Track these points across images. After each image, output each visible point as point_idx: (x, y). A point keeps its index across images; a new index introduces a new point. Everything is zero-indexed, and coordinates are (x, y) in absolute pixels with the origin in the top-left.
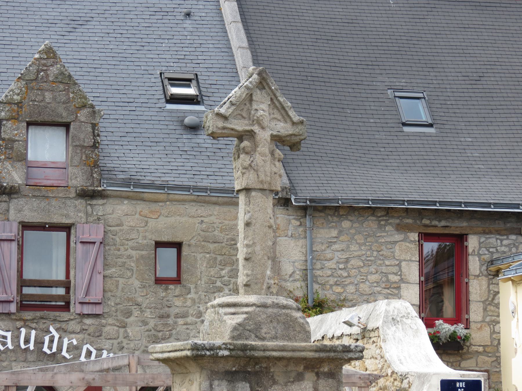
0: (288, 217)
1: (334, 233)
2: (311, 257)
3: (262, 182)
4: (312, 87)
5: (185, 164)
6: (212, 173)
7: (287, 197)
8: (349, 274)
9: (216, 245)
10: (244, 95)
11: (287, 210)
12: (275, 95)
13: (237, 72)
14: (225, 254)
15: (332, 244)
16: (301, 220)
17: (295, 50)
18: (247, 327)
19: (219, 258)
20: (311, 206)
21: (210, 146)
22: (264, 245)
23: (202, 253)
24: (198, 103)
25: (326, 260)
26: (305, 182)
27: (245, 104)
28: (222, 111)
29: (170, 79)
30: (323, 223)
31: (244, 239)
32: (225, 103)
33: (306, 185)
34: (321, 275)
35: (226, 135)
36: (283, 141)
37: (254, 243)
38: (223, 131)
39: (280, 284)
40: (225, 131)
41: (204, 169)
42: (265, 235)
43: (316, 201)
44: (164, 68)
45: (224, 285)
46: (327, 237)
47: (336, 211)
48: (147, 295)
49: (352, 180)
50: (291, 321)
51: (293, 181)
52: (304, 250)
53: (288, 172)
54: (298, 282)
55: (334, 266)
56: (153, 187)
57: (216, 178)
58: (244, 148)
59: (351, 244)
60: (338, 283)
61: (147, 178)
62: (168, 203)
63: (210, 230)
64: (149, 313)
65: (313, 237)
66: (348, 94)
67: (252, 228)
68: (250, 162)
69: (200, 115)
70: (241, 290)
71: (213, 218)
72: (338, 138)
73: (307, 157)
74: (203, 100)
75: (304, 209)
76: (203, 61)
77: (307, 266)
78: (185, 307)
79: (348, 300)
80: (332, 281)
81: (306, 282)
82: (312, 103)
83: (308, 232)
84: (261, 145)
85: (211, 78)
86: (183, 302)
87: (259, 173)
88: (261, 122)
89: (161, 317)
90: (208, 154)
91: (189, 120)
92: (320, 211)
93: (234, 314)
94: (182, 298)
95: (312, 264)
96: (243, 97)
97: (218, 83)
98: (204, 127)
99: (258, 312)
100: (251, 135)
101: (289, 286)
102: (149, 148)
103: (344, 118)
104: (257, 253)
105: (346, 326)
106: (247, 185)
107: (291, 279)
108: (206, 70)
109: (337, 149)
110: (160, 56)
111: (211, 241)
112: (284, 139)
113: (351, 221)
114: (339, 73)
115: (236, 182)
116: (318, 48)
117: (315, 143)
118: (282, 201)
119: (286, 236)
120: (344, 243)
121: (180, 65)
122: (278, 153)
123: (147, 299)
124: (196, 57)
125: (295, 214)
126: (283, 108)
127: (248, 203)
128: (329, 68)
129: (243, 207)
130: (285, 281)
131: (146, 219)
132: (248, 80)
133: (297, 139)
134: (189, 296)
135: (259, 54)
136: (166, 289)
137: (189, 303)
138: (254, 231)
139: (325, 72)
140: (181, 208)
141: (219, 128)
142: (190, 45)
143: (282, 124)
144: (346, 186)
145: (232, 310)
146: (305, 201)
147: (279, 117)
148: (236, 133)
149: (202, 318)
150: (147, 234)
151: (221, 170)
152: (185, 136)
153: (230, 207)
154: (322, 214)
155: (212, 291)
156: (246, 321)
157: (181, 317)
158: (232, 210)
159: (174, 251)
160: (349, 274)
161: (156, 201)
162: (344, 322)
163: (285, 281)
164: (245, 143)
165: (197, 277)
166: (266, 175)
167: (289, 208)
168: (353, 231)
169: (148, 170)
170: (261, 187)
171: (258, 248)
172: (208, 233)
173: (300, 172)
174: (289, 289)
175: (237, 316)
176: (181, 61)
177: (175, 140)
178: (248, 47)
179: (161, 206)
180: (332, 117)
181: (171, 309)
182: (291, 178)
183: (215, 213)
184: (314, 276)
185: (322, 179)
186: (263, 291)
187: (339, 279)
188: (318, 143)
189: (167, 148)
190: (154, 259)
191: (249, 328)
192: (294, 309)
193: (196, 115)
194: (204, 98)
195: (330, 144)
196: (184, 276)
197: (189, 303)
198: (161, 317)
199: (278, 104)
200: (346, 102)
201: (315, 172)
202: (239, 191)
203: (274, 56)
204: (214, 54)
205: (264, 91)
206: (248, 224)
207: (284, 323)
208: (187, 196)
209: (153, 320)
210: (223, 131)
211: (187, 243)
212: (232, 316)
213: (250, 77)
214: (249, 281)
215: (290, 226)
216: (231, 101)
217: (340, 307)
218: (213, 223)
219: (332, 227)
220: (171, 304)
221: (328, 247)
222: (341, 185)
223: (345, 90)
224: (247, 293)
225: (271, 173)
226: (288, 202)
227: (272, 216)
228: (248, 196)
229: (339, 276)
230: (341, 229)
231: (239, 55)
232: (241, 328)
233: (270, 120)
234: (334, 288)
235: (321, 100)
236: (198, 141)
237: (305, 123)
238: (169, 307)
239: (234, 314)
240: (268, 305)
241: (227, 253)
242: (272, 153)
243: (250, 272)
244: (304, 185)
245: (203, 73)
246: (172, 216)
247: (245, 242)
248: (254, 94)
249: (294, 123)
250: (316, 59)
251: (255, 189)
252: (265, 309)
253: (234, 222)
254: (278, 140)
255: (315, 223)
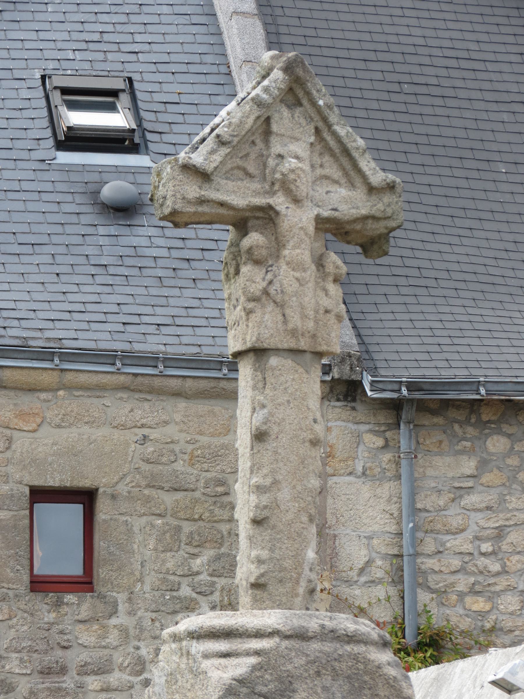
0: (354, 427)
1: (469, 465)
2: (411, 525)
3: (294, 333)
4: (413, 109)
5: (104, 298)
6: (169, 321)
7: (354, 377)
8: (504, 566)
9: (179, 495)
10: (250, 121)
11: (353, 409)
12: (325, 120)
13: (229, 74)
14: (200, 519)
15: (462, 492)
16: (388, 434)
17: (370, 18)
18: (260, 688)
19: (187, 527)
20: (411, 401)
21: (164, 253)
22: (299, 488)
23: (144, 514)
24: (134, 149)
25: (448, 532)
26: (396, 340)
27: (253, 142)
28: (198, 158)
29: (65, 91)
30: (441, 442)
31: (252, 472)
32: (203, 140)
33: (400, 348)
34: (437, 569)
35: (207, 218)
36: (346, 233)
37: (275, 482)
38: (200, 209)
39: (335, 591)
40: (205, 209)
41: (148, 310)
42: (303, 462)
43: (425, 387)
44: (51, 65)
45: (199, 593)
46: (450, 475)
47: (472, 411)
48: (10, 619)
49: (511, 335)
50: (366, 672)
51: (367, 340)
52: (394, 508)
53: (354, 317)
54: (379, 587)
55: (468, 547)
56: (26, 355)
57: (179, 331)
58: (250, 251)
59: (509, 494)
60: (477, 588)
61: (11, 332)
62: (61, 393)
63: (164, 459)
64: (17, 662)
65: (416, 475)
66: (499, 127)
67: (271, 444)
68: (264, 284)
69: (141, 179)
70: (245, 598)
71: (171, 430)
72: (476, 233)
73: (402, 281)
74: (146, 141)
75: (395, 406)
76: (147, 47)
77: (401, 546)
78: (105, 647)
79: (501, 629)
80: (463, 583)
81: (400, 587)
82: (413, 148)
83: (404, 463)
84: (291, 243)
85: (166, 87)
86: (99, 637)
87: (288, 311)
88: (292, 187)
89: (46, 672)
90: (160, 273)
91: (110, 191)
92: (434, 413)
93: (226, 655)
94: (96, 627)
95: (415, 542)
96: (248, 126)
97: (184, 99)
98: (151, 200)
99: (286, 652)
100: (267, 216)
101: (359, 595)
102: (16, 259)
103: (490, 186)
104: (282, 507)
105: (498, 691)
106: (258, 339)
107: (363, 579)
108: (153, 68)
109: (474, 260)
110: (42, 35)
111: (167, 486)
112: (348, 227)
113: (509, 436)
114: (480, 75)
115: (231, 334)
116: (426, 14)
117: (420, 245)
118: (342, 388)
119: (350, 474)
120: (492, 491)
121: (89, 56)
122: (333, 259)
123: (10, 627)
124: (129, 38)
125: (372, 420)
126: (346, 152)
127: (261, 384)
128: (453, 63)
129: (249, 393)
130: (349, 582)
131: (8, 432)
132: (259, 83)
133: (380, 227)
134: (114, 621)
135: (283, 30)
136: (58, 604)
137: (113, 638)
138: (276, 453)
139: (443, 72)
140: (93, 405)
141: (189, 202)
142: (114, 9)
143: (343, 192)
144: (496, 350)
145: (222, 646)
146: (396, 387)
147: (336, 173)
148: (231, 213)
149: (145, 675)
150: (11, 469)
151: (192, 312)
152: (102, 230)
153: (213, 402)
154: (439, 420)
155: (170, 607)
156: (258, 674)
157: (96, 673)
158: (217, 409)
159: (76, 511)
160: (504, 566)
161: (32, 389)
162: (494, 683)
163: (349, 582)
164: (254, 238)
165: (132, 573)
166: (304, 317)
167: (358, 405)
168: (513, 461)
169: (12, 314)
170: (292, 345)
171: (284, 494)
172: (161, 467)
173: (383, 316)
174: (357, 604)
175: (233, 661)
176: (92, 46)
177: (79, 240)
178: (256, 12)
179: (45, 401)
180: (463, 183)
181: (68, 652)
182: (363, 332)
183: (178, 417)
184: (419, 572)
185: (437, 333)
186: (298, 600)
187: (480, 578)
188: (429, 246)
189: (59, 259)
190: (28, 531)
191: (264, 690)
192: (374, 643)
193: (131, 177)
194: (149, 136)
195: (456, 249)
196: (101, 572)
197: (113, 638)
198: (46, 672)
199: (332, 143)
200: (494, 147)
201: (421, 317)
202: (238, 355)
203: (321, 33)
204: (173, 29)
205: (298, 111)
206: (260, 437)
207: (348, 677)
208: (109, 376)
209: (27, 678)
210: (200, 209)
211: (109, 491)
212: (223, 661)
213: (264, 77)
214: (262, 575)
215: (361, 448)
216: (218, 136)
217: (483, 648)
218: (172, 442)
219: (462, 452)
220: (68, 641)
221: (453, 500)
222: (484, 349)
223: (494, 116)
224: (258, 604)
225: (317, 312)
226: (355, 391)
227: (318, 416)
228: (260, 368)
229: (481, 573)
230: (484, 455)
231: (235, 31)
232: (244, 690)
233: (314, 182)
234: (468, 600)
235: (434, 141)
236: (135, 241)
237: (399, 189)
238: (65, 648)
239: (226, 655)
240: (310, 634)
241: (207, 514)
242: (320, 263)
243: (265, 554)
244: (394, 348)
245: (147, 77)
246: (70, 425)
247: (254, 480)
248: (276, 117)
249: (371, 190)
250: (421, 41)
251: (277, 351)
252: (304, 644)
253: (224, 440)
254: (334, 229)
255: (421, 440)
